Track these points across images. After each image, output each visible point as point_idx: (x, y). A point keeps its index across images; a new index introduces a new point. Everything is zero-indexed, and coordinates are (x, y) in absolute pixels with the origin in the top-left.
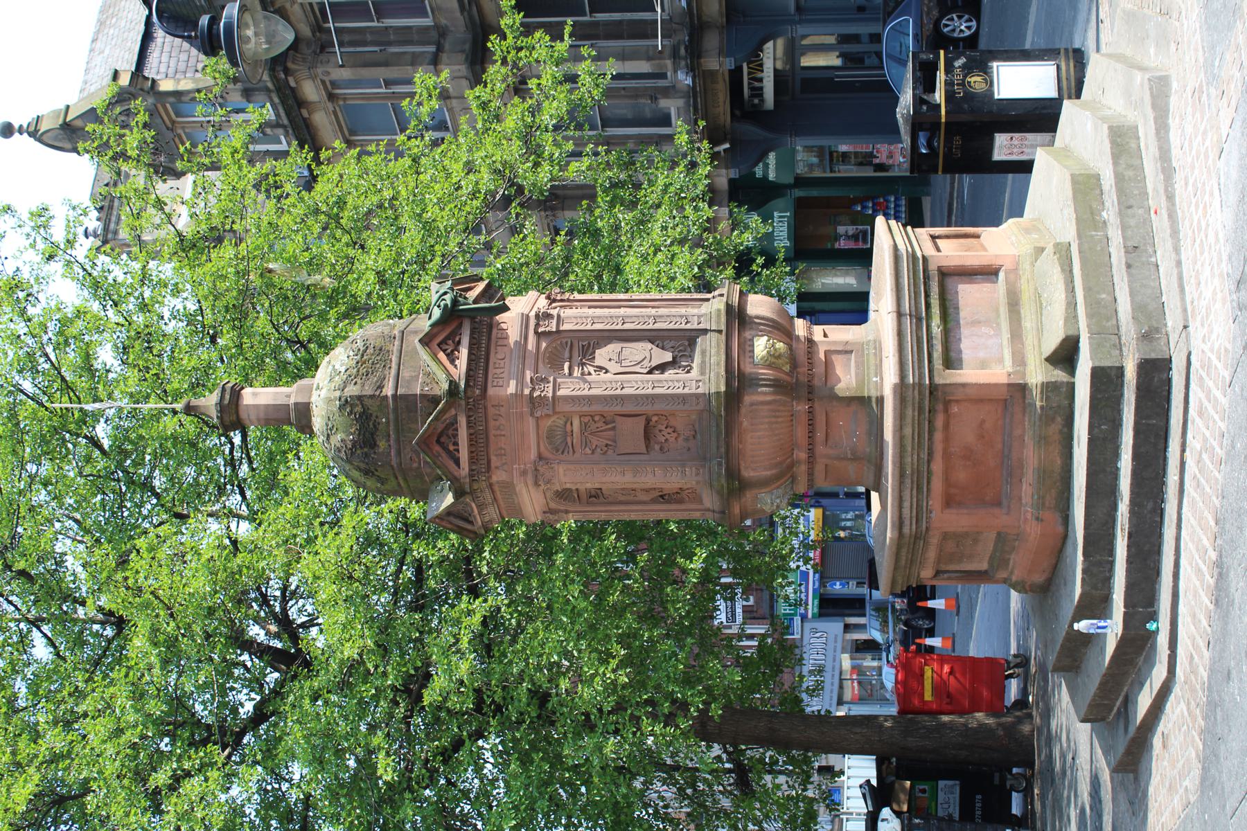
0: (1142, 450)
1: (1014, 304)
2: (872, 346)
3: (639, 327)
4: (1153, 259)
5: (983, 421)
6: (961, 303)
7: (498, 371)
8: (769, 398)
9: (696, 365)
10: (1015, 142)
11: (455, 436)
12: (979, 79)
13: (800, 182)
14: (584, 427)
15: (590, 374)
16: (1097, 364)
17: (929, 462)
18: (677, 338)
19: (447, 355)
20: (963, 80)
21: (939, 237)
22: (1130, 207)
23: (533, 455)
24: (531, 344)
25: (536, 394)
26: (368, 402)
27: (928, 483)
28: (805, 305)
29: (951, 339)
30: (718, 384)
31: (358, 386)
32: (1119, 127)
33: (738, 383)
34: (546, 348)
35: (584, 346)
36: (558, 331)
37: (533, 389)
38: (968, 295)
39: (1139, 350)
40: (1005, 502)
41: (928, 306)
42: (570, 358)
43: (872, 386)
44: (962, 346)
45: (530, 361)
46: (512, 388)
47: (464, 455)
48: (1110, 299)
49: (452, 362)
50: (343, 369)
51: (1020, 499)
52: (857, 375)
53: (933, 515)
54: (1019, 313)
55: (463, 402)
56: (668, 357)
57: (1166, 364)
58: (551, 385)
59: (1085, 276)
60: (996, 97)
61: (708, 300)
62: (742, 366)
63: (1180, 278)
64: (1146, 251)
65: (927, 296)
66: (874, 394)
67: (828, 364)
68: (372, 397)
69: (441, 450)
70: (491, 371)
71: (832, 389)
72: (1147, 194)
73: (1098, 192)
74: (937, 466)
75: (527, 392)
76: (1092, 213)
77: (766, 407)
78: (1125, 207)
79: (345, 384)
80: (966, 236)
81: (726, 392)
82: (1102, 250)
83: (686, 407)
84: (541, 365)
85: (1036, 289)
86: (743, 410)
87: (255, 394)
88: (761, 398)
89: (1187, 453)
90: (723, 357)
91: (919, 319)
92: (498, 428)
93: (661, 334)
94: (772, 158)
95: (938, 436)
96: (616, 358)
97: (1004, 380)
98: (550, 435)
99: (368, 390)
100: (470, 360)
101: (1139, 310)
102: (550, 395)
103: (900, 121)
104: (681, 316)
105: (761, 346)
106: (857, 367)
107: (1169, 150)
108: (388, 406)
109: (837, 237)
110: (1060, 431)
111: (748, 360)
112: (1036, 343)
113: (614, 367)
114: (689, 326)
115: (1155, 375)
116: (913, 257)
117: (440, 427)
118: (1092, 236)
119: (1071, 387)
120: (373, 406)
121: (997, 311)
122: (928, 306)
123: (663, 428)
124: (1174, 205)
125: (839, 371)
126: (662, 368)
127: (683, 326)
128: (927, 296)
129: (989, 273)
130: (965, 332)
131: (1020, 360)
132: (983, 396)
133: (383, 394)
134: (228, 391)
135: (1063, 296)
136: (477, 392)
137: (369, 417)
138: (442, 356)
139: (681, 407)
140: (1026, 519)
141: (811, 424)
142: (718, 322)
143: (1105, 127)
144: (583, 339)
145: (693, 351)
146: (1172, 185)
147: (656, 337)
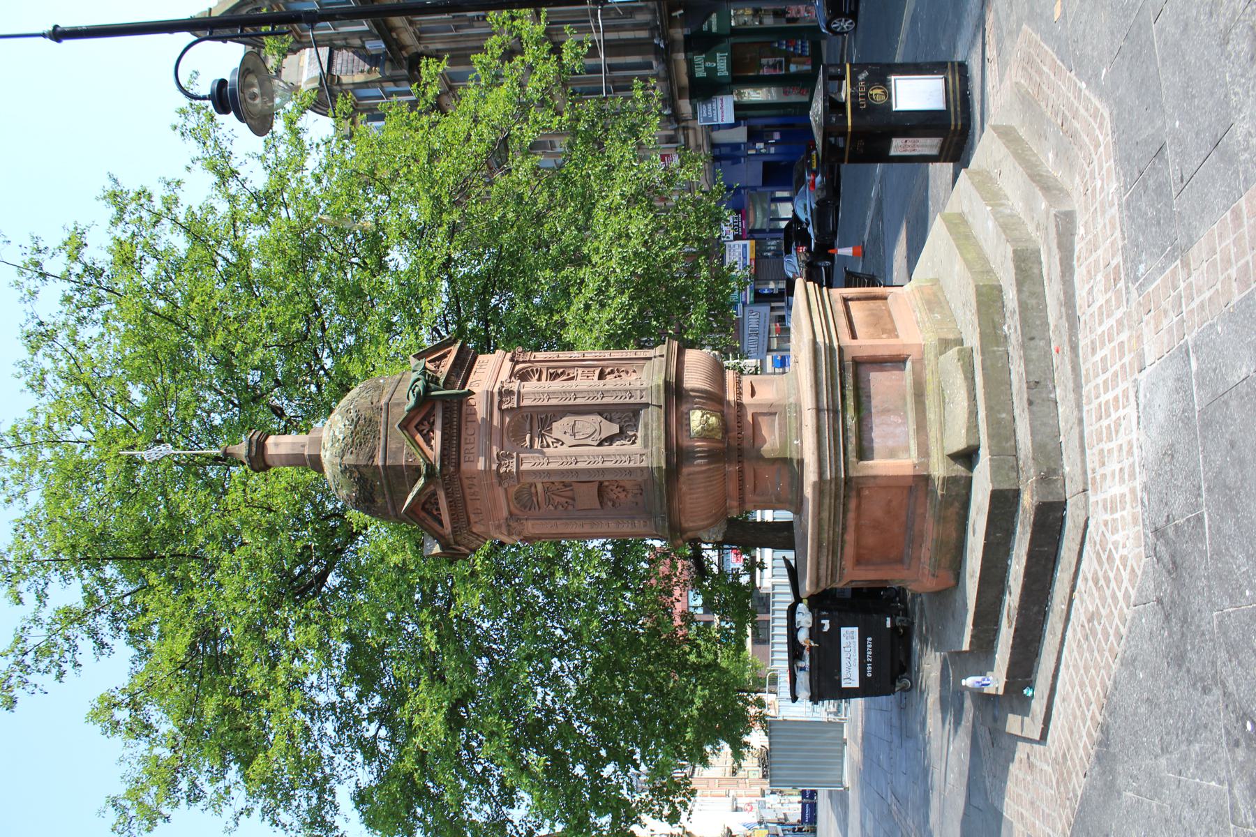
1: (919, 395)
5: (890, 501)
7: (469, 446)
13: (735, 32)
14: (546, 490)
15: (548, 446)
16: (997, 487)
18: (623, 411)
19: (423, 436)
21: (852, 299)
22: (1032, 339)
23: (505, 513)
26: (364, 470)
29: (864, 428)
30: (659, 462)
31: (354, 456)
33: (677, 456)
35: (541, 419)
36: (519, 407)
37: (500, 465)
38: (879, 381)
42: (531, 430)
45: (496, 437)
47: (446, 518)
48: (1009, 418)
49: (428, 442)
50: (341, 437)
51: (919, 559)
54: (923, 403)
56: (615, 429)
57: (1062, 505)
61: (650, 359)
63: (1082, 438)
64: (1046, 386)
65: (843, 387)
66: (795, 456)
67: (755, 425)
68: (366, 466)
71: (759, 450)
72: (1048, 324)
73: (1000, 304)
74: (850, 537)
75: (494, 467)
76: (994, 327)
78: (1028, 339)
82: (1003, 366)
84: (505, 439)
86: (682, 479)
89: (1076, 594)
90: (663, 427)
91: (835, 412)
94: (714, 17)
95: (851, 515)
96: (569, 431)
98: (518, 498)
99: (362, 462)
103: (813, 124)
105: (696, 419)
107: (1073, 295)
109: (761, 66)
111: (685, 434)
113: (569, 440)
114: (632, 401)
115: (1050, 521)
116: (830, 349)
117: (423, 499)
118: (994, 352)
119: (969, 481)
120: (368, 473)
121: (904, 399)
124: (1077, 356)
125: (765, 432)
126: (610, 440)
127: (627, 401)
128: (843, 387)
129: (898, 362)
131: (924, 451)
138: (419, 438)
140: (923, 574)
141: (741, 480)
142: (658, 398)
143: (1010, 250)
144: (541, 413)
145: (637, 420)
147: (605, 411)
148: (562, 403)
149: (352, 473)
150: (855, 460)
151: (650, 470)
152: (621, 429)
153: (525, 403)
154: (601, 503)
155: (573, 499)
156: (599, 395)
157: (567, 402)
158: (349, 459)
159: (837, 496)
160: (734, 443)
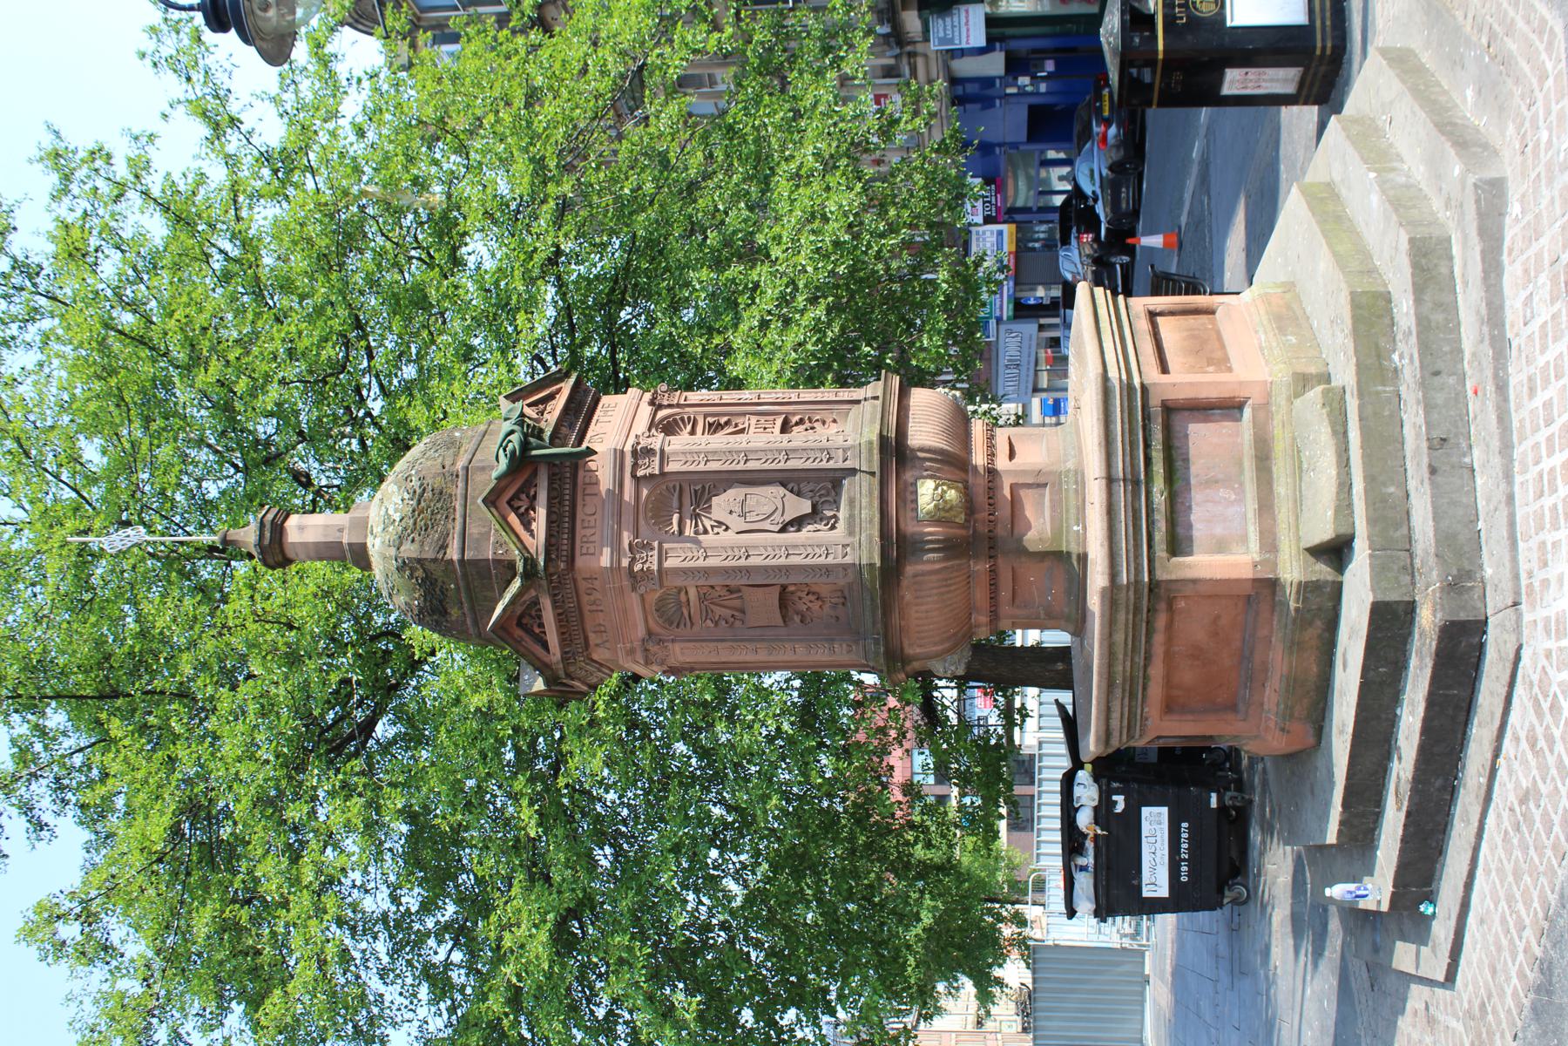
0: (1436, 723)
2: (1072, 480)
4: (1467, 460)
5: (1218, 617)
6: (1192, 452)
7: (588, 532)
8: (937, 566)
10: (1250, 76)
11: (540, 617)
14: (702, 598)
15: (706, 532)
16: (1380, 598)
17: (1145, 667)
18: (818, 480)
19: (520, 516)
21: (1161, 314)
22: (1437, 373)
23: (641, 632)
24: (628, 494)
25: (637, 567)
26: (432, 567)
27: (1144, 689)
28: (995, 31)
29: (1179, 507)
30: (870, 552)
32: (1423, 239)
33: (898, 547)
34: (648, 496)
35: (697, 491)
36: (663, 474)
38: (1202, 438)
40: (1241, 707)
41: (1148, 461)
43: (1072, 539)
45: (628, 518)
47: (553, 638)
48: (1401, 494)
49: (527, 525)
50: (397, 517)
51: (1262, 704)
53: (1149, 723)
55: (544, 583)
56: (805, 507)
58: (656, 552)
60: (1229, 24)
61: (858, 402)
62: (902, 526)
63: (1512, 524)
65: (1147, 446)
66: (1074, 549)
67: (1015, 502)
68: (435, 560)
71: (1020, 540)
72: (1461, 351)
73: (1387, 321)
74: (1157, 671)
75: (625, 563)
76: (1379, 356)
77: (934, 578)
79: (401, 540)
80: (1197, 311)
81: (881, 568)
82: (1391, 416)
83: (831, 579)
84: (642, 522)
85: (1294, 439)
86: (905, 583)
87: (301, 528)
89: (1501, 761)
90: (876, 503)
92: (594, 603)
93: (796, 475)
95: (1159, 638)
96: (737, 509)
98: (661, 607)
99: (429, 553)
100: (550, 522)
105: (927, 492)
106: (1053, 508)
107: (1501, 307)
108: (454, 571)
110: (1319, 636)
111: (910, 514)
113: (736, 523)
114: (831, 465)
115: (1462, 650)
116: (1130, 387)
118: (1378, 393)
120: (437, 571)
121: (1240, 464)
122: (1148, 461)
123: (803, 595)
124: (1506, 400)
125: (1029, 512)
126: (798, 523)
127: (824, 465)
128: (1147, 446)
129: (1230, 408)
131: (1269, 543)
133: (448, 557)
134: (268, 526)
135: (1334, 473)
136: (562, 566)
137: (434, 583)
138: (513, 519)
139: (824, 579)
140: (1267, 728)
142: (870, 461)
145: (838, 494)
146: (1505, 368)
147: (790, 480)
148: (726, 467)
149: (413, 570)
150: (1164, 555)
152: (814, 506)
153: (672, 467)
154: (784, 617)
156: (782, 457)
157: (734, 467)
158: (410, 550)
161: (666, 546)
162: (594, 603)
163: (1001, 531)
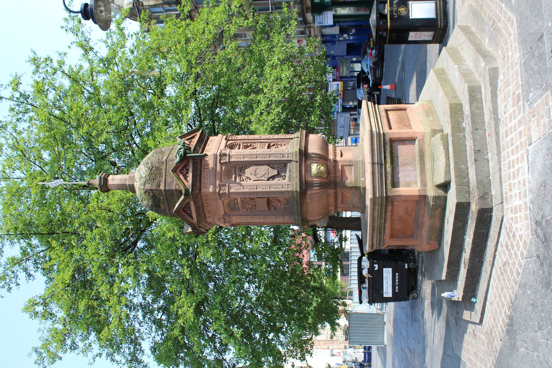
3: (263, 159)
4: (486, 157)
5: (407, 207)
6: (399, 154)
7: (205, 181)
8: (318, 191)
9: (287, 175)
10: (418, 34)
11: (190, 208)
12: (403, 9)
14: (242, 202)
15: (243, 180)
16: (459, 201)
17: (384, 223)
18: (279, 164)
19: (183, 176)
20: (397, 10)
21: (389, 110)
22: (477, 129)
23: (223, 213)
24: (218, 169)
25: (221, 192)
26: (155, 192)
27: (384, 230)
28: (336, 20)
29: (395, 172)
30: (296, 188)
33: (305, 185)
35: (240, 168)
36: (229, 162)
37: (220, 190)
38: (402, 150)
39: (479, 204)
42: (235, 173)
43: (361, 182)
44: (399, 176)
45: (218, 176)
46: (211, 189)
47: (194, 215)
48: (465, 168)
49: (186, 178)
50: (144, 176)
51: (422, 235)
52: (355, 176)
54: (424, 161)
55: (191, 197)
56: (275, 172)
57: (491, 210)
58: (227, 187)
59: (455, 156)
60: (411, 18)
61: (292, 139)
62: (306, 178)
65: (385, 153)
66: (362, 186)
67: (343, 171)
69: (185, 214)
70: (203, 181)
71: (344, 183)
72: (484, 122)
73: (461, 113)
74: (388, 225)
75: (217, 190)
78: (475, 129)
79: (145, 183)
80: (401, 110)
84: (223, 177)
85: (432, 150)
86: (307, 197)
88: (315, 192)
89: (497, 253)
90: (298, 171)
95: (389, 214)
96: (254, 173)
97: (417, 193)
98: (229, 205)
99: (154, 188)
101: (480, 182)
102: (227, 192)
103: (371, 25)
104: (281, 154)
105: (314, 168)
106: (355, 172)
110: (440, 214)
111: (309, 175)
112: (431, 176)
113: (253, 177)
114: (284, 159)
115: (485, 217)
116: (379, 134)
118: (458, 136)
119: (445, 198)
120: (157, 193)
121: (414, 158)
124: (499, 138)
125: (347, 174)
126: (273, 177)
127: (281, 159)
128: (385, 153)
129: (411, 140)
130: (401, 169)
132: (407, 199)
133: (160, 189)
136: (197, 191)
138: (181, 176)
139: (281, 196)
142: (296, 158)
145: (286, 168)
146: (498, 128)
147: (270, 164)
150: (390, 187)
151: (292, 192)
152: (278, 172)
153: (232, 160)
154: (268, 208)
155: (255, 206)
156: (268, 156)
158: (148, 186)
159: (382, 205)
160: (332, 179)
161: (230, 185)
162: (207, 203)
163: (338, 180)
